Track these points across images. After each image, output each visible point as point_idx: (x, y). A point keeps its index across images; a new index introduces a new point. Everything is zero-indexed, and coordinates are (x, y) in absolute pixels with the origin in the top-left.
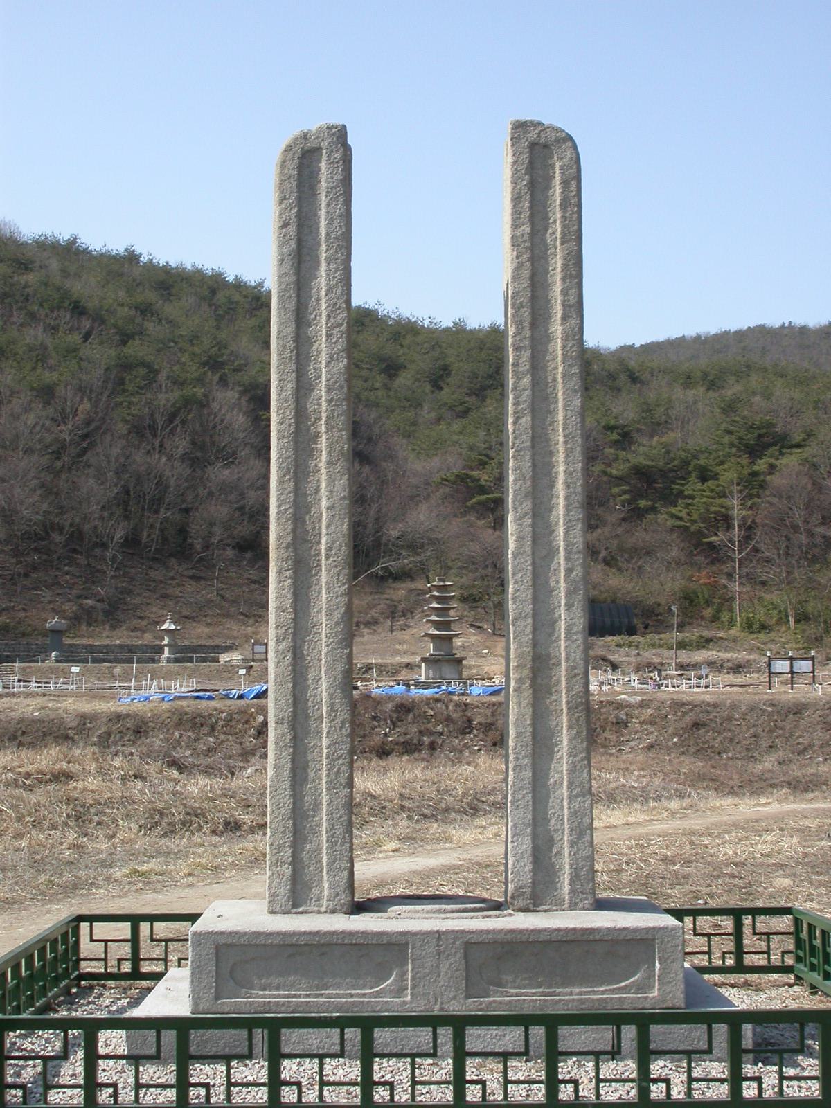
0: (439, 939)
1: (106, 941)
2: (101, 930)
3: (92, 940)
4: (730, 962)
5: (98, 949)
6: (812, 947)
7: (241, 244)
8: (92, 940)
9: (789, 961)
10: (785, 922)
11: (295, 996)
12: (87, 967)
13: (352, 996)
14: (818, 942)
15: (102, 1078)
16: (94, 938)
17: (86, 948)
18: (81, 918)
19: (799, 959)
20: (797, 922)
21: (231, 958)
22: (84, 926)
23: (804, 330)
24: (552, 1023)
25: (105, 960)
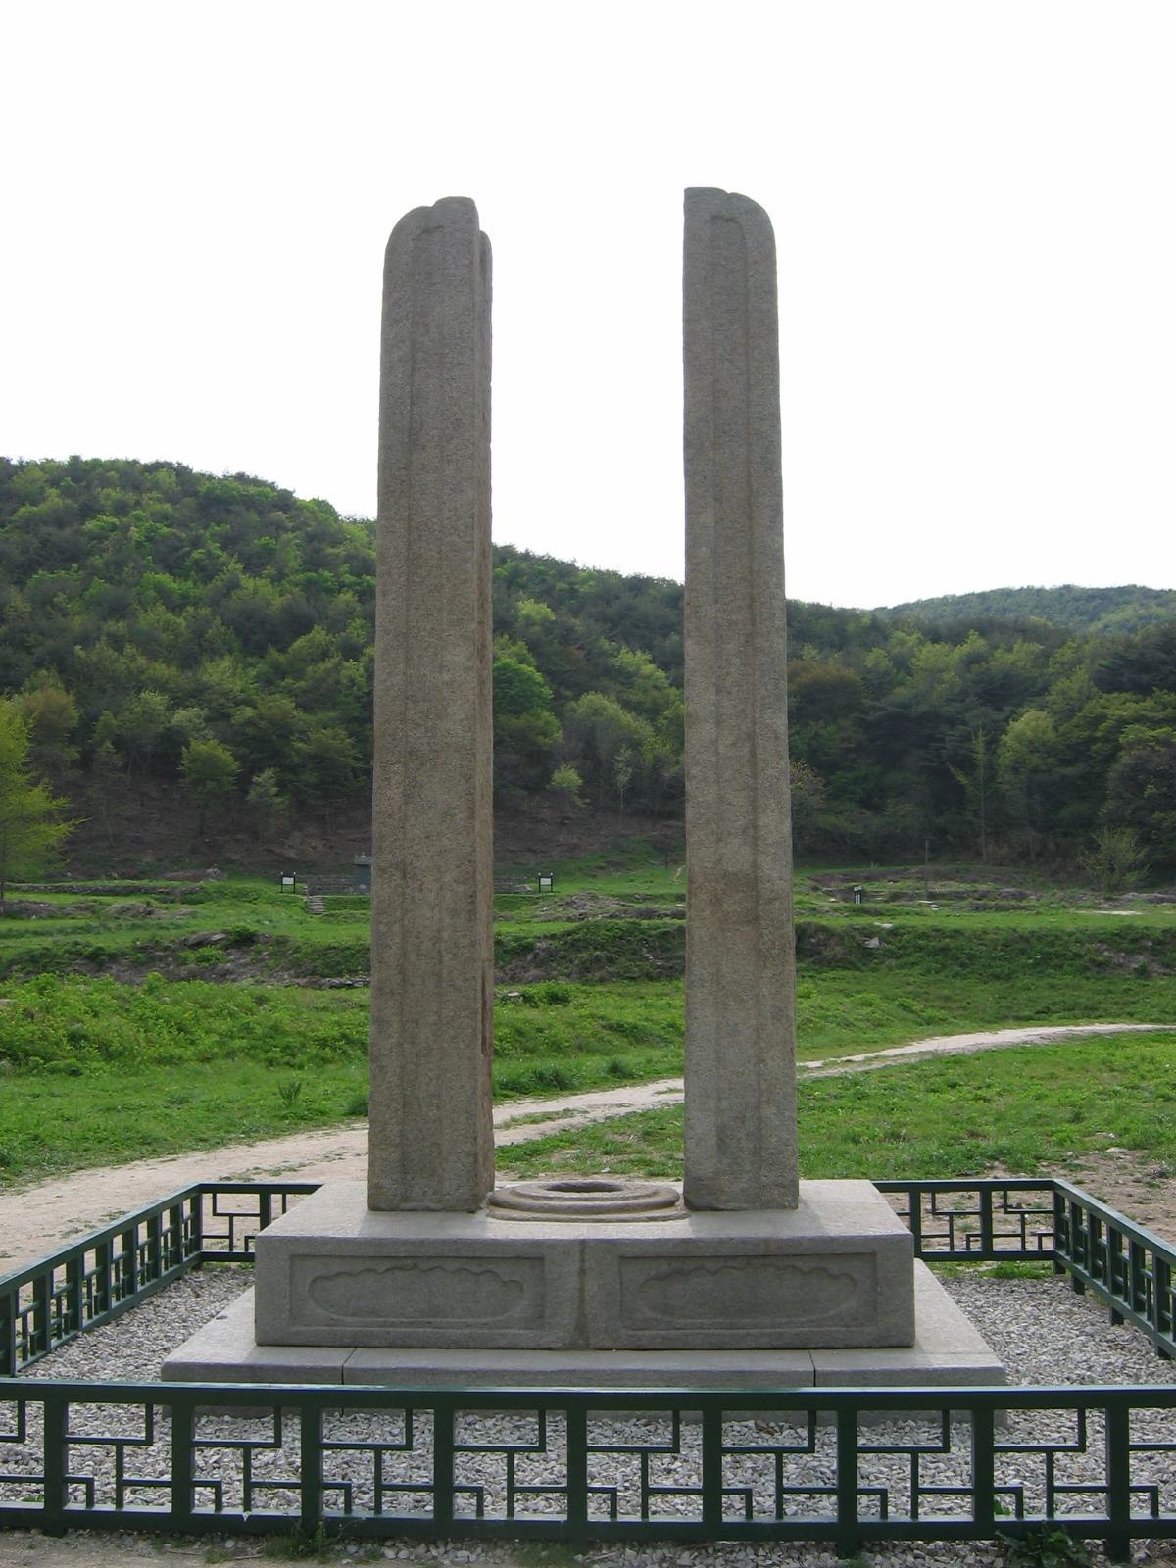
0: (582, 1252)
1: (231, 1216)
2: (227, 1202)
3: (215, 1214)
4: (976, 1247)
5: (220, 1227)
6: (1078, 1233)
7: (330, 458)
8: (215, 1214)
9: (1049, 1245)
10: (1046, 1199)
11: (393, 1324)
12: (208, 1247)
13: (469, 1326)
14: (1085, 1226)
15: (73, 1465)
16: (218, 1211)
17: (211, 1225)
18: (203, 1188)
19: (1059, 1244)
20: (1059, 1201)
21: (303, 1284)
22: (207, 1199)
23: (1040, 592)
24: (578, 1409)
25: (230, 1237)
